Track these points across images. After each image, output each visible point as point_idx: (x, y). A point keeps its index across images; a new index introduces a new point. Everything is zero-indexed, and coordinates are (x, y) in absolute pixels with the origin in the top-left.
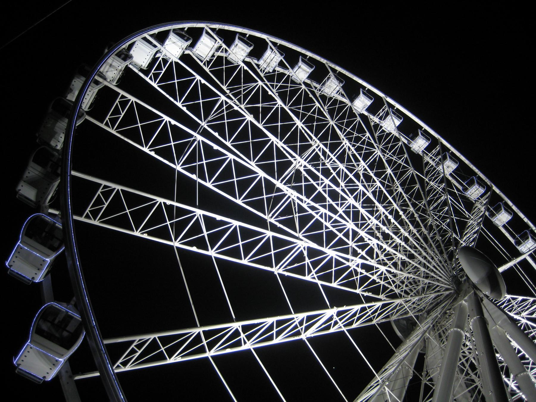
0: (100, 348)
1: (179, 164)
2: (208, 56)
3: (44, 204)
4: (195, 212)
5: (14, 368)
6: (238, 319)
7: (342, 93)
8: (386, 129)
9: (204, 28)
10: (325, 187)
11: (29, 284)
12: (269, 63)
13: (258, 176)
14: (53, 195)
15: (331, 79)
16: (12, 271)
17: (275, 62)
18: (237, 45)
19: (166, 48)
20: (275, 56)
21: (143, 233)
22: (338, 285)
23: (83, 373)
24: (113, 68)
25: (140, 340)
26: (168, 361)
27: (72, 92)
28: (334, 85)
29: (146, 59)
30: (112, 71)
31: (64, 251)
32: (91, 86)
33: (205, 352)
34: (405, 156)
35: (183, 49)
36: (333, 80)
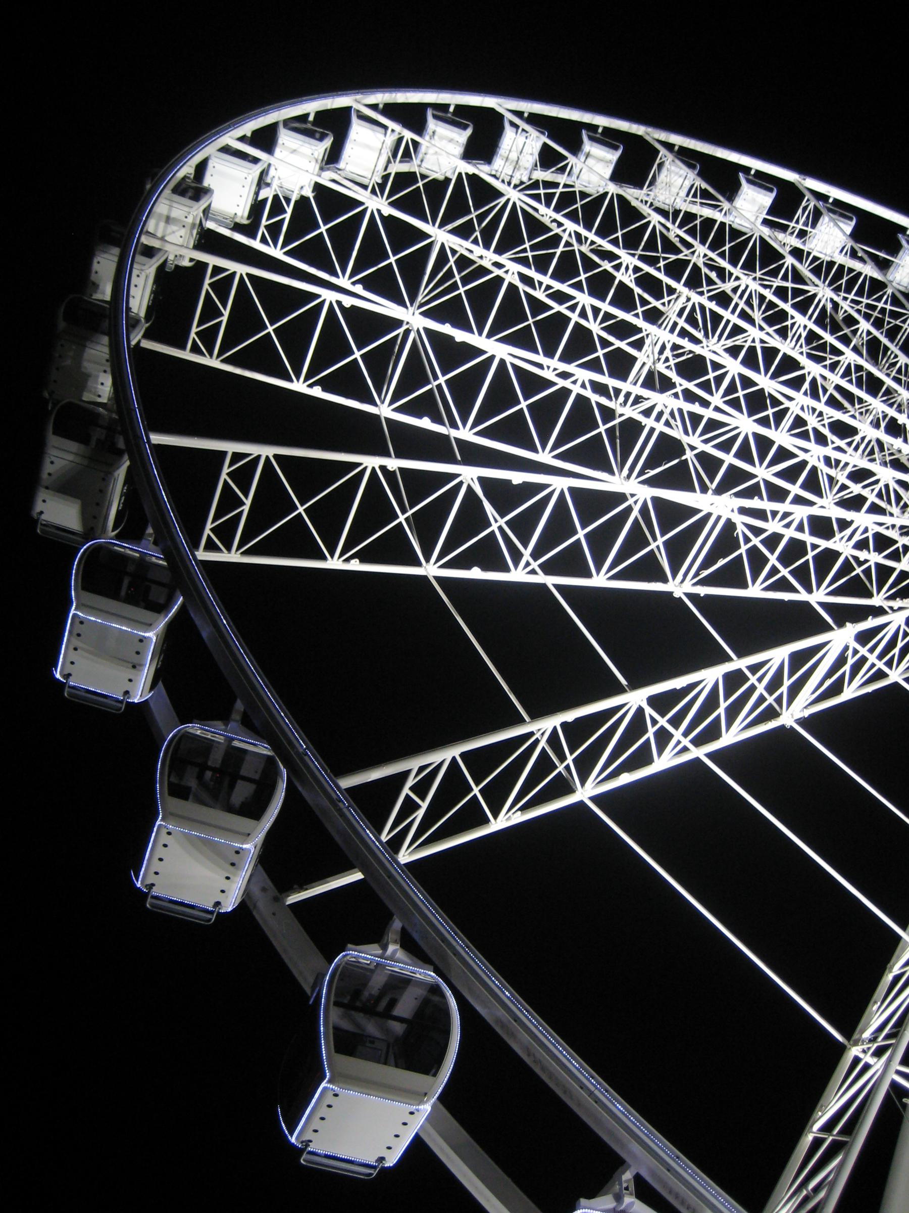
0: (334, 796)
1: (383, 402)
2: (378, 172)
3: (104, 533)
4: (459, 475)
5: (142, 896)
6: (635, 685)
7: (700, 187)
8: (821, 253)
9: (350, 108)
10: (732, 389)
11: (121, 712)
12: (517, 162)
13: (552, 450)
14: (120, 508)
15: (667, 164)
16: (74, 688)
17: (531, 154)
18: (434, 133)
19: (285, 144)
20: (527, 141)
21: (347, 560)
22: (830, 594)
23: (302, 887)
24: (176, 225)
25: (422, 769)
26: (492, 826)
27: (99, 291)
28: (676, 177)
29: (238, 206)
30: (174, 232)
31: (183, 608)
32: (137, 263)
33: (570, 790)
34: (888, 293)
35: (317, 161)
36: (673, 168)
